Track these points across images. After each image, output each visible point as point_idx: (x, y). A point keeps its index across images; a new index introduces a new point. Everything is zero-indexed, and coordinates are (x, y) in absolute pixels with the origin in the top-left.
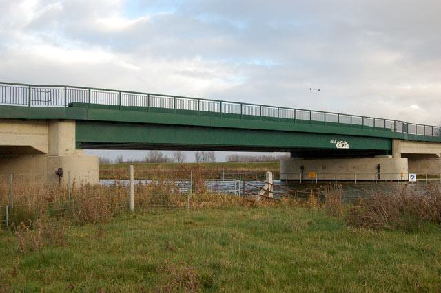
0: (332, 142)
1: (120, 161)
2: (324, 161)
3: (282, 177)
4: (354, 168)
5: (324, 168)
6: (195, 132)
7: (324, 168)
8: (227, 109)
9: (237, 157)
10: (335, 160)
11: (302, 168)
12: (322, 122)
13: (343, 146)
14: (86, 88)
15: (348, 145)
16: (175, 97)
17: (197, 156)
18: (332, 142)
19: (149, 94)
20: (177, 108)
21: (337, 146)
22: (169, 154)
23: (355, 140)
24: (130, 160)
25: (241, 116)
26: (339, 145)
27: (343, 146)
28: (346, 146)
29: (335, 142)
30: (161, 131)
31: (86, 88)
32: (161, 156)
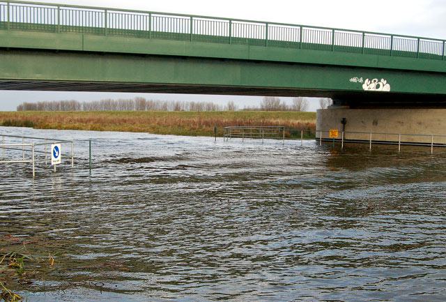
0: (354, 80)
1: (231, 106)
2: (377, 111)
3: (319, 135)
4: (420, 123)
5: (375, 123)
6: (111, 64)
7: (375, 123)
8: (399, 46)
9: (199, 106)
10: (394, 111)
11: (344, 122)
12: (295, 44)
13: (378, 86)
14: (297, 26)
15: (388, 85)
16: (301, 26)
17: (322, 104)
18: (354, 80)
19: (333, 29)
20: (336, 43)
21: (365, 88)
22: (288, 101)
23: (399, 76)
24: (247, 108)
25: (417, 55)
26: (369, 86)
27: (378, 86)
28: (385, 87)
29: (361, 80)
30: (170, 66)
31: (297, 26)
32: (278, 103)
